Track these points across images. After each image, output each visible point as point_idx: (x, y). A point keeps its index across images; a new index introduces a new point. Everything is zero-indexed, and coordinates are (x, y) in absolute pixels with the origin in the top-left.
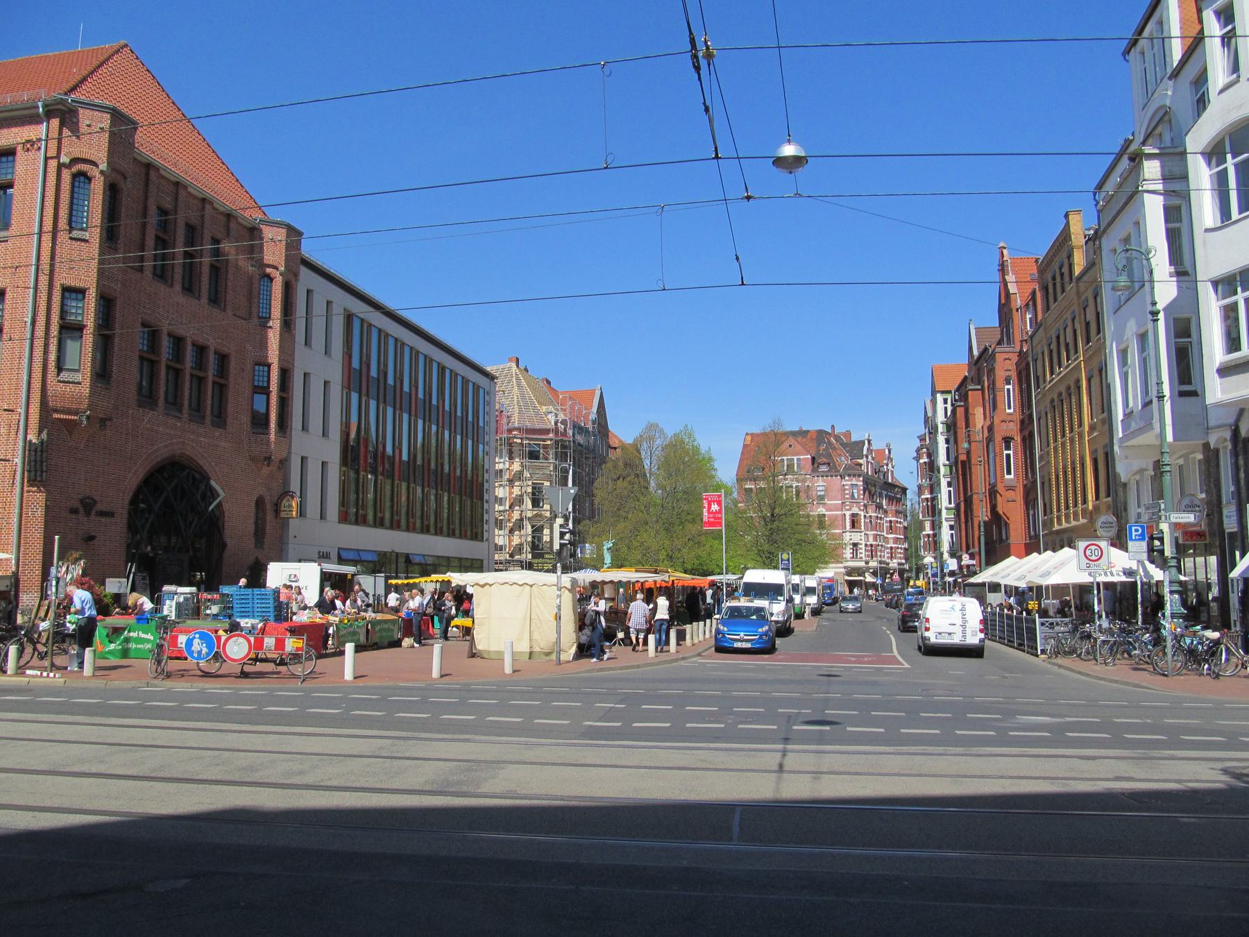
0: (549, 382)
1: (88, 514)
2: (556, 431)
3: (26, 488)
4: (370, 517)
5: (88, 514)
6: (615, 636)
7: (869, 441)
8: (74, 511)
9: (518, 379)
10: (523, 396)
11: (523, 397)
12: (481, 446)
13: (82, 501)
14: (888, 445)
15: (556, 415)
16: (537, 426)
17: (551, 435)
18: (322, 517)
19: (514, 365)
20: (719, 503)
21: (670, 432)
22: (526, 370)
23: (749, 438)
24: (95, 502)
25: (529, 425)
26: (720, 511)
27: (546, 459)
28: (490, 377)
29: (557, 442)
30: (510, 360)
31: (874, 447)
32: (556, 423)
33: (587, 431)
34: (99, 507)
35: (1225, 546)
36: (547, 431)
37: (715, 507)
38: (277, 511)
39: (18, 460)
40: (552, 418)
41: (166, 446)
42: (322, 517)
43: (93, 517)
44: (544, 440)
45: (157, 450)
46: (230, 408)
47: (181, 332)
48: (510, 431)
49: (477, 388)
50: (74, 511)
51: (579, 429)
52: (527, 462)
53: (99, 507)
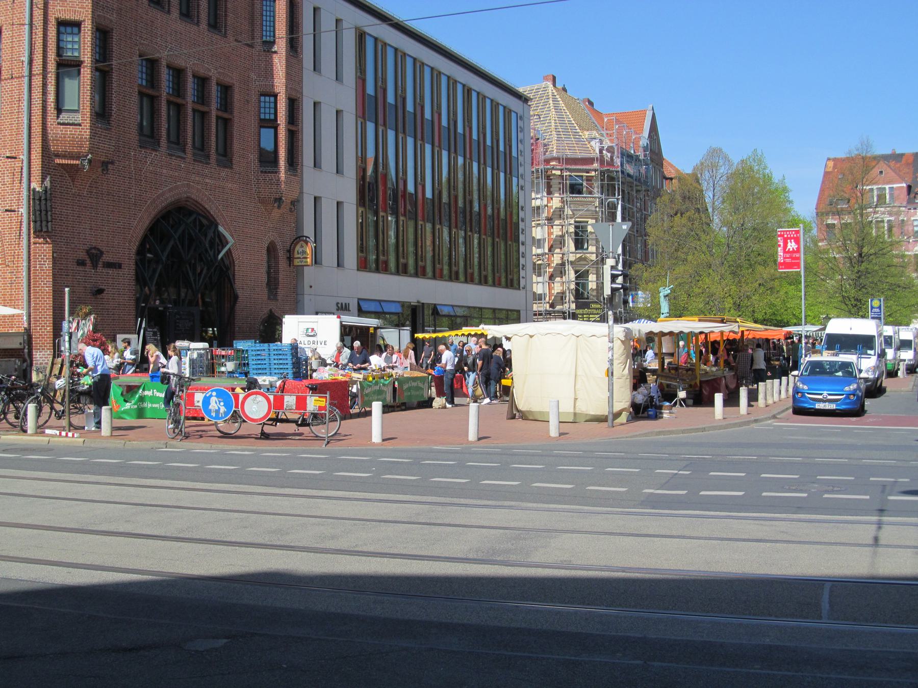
1: (95, 266)
2: (601, 160)
3: (32, 240)
5: (95, 266)
8: (81, 263)
9: (555, 100)
10: (561, 118)
12: (515, 180)
13: (88, 252)
15: (601, 142)
16: (579, 155)
17: (596, 165)
20: (797, 241)
21: (736, 159)
22: (564, 90)
23: (831, 164)
24: (102, 253)
25: (569, 154)
34: (106, 258)
36: (590, 161)
37: (792, 245)
38: (290, 259)
39: (23, 210)
40: (596, 145)
41: (170, 190)
43: (100, 269)
45: (162, 194)
46: (236, 145)
47: (180, 63)
48: (547, 161)
49: (508, 112)
50: (81, 263)
51: (629, 158)
52: (568, 196)
53: (106, 258)
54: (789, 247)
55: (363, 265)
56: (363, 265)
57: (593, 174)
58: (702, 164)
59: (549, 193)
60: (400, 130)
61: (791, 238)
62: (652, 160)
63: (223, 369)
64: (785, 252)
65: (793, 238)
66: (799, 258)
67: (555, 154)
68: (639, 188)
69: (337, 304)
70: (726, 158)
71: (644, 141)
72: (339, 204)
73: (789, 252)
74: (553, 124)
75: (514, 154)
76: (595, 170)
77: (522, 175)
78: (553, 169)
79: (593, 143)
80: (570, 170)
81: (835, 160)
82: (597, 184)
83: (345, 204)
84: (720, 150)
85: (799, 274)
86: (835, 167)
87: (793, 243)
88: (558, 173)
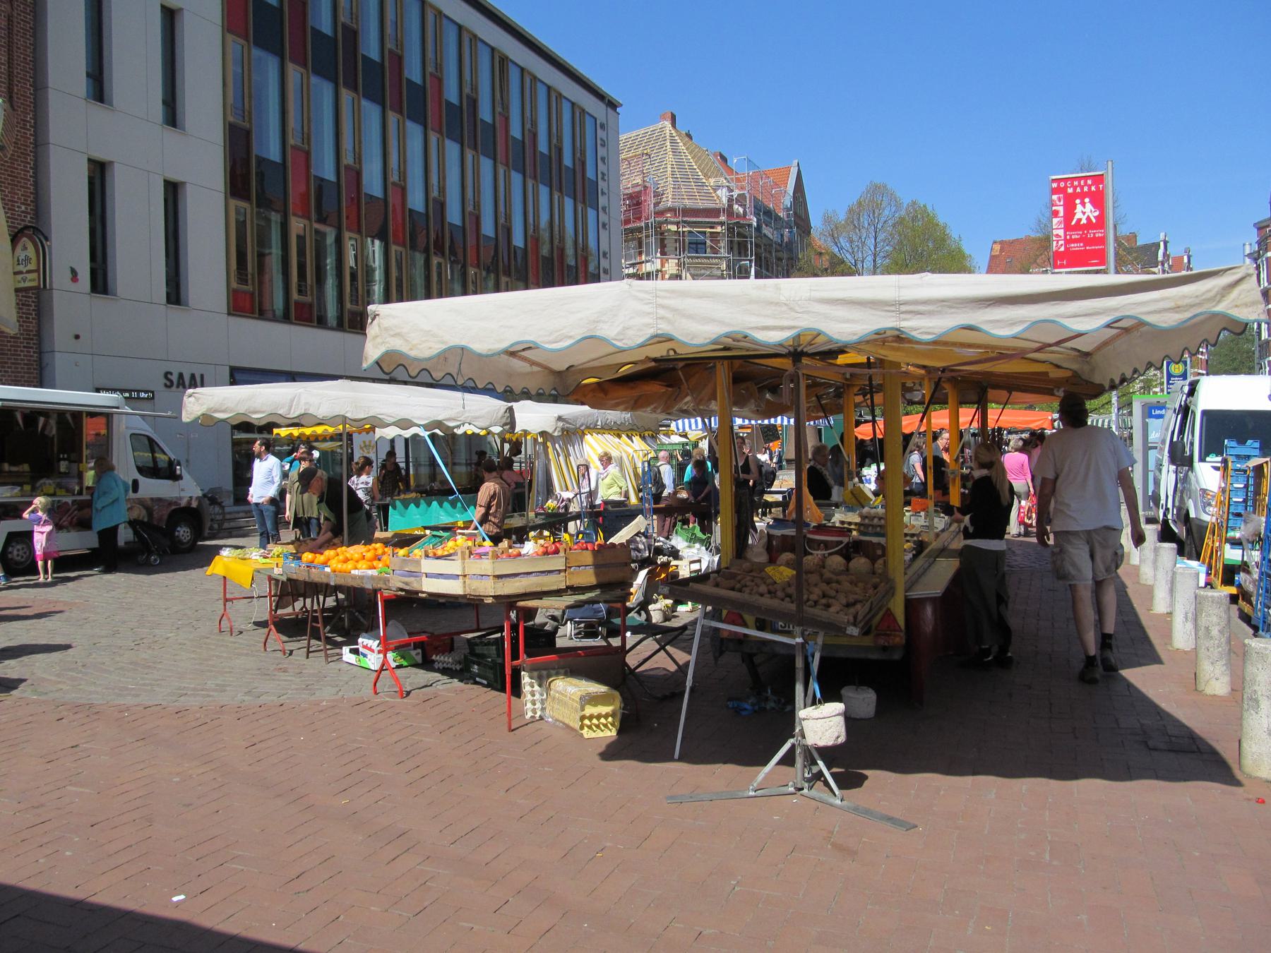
0: (724, 159)
2: (729, 211)
4: (331, 312)
6: (786, 724)
7: (1166, 243)
9: (673, 142)
10: (680, 165)
11: (680, 165)
12: (591, 213)
14: (1187, 251)
15: (730, 190)
16: (701, 205)
17: (723, 218)
18: (175, 295)
19: (668, 124)
21: (906, 201)
22: (689, 136)
23: (997, 247)
25: (688, 203)
26: (1101, 219)
27: (715, 251)
28: (612, 105)
29: (730, 230)
30: (663, 118)
31: (1172, 251)
32: (730, 200)
33: (778, 218)
35: (12, 537)
36: (715, 212)
40: (723, 195)
42: (175, 295)
44: (712, 225)
48: (660, 213)
49: (579, 112)
51: (766, 214)
52: (686, 257)
54: (1078, 215)
55: (246, 303)
56: (246, 303)
57: (719, 229)
58: (860, 204)
59: (663, 253)
60: (326, 70)
61: (1082, 196)
62: (796, 223)
63: (664, 439)
64: (1068, 227)
65: (1089, 194)
66: (1102, 241)
67: (669, 204)
68: (780, 254)
69: (167, 375)
70: (893, 198)
71: (788, 201)
72: (173, 190)
73: (1078, 226)
74: (669, 169)
75: (590, 174)
76: (722, 224)
77: (604, 209)
78: (667, 222)
79: (719, 192)
80: (689, 224)
81: (1002, 243)
82: (723, 244)
83: (189, 188)
84: (885, 186)
85: (502, 637)
86: (1002, 250)
87: (1089, 207)
88: (674, 228)
